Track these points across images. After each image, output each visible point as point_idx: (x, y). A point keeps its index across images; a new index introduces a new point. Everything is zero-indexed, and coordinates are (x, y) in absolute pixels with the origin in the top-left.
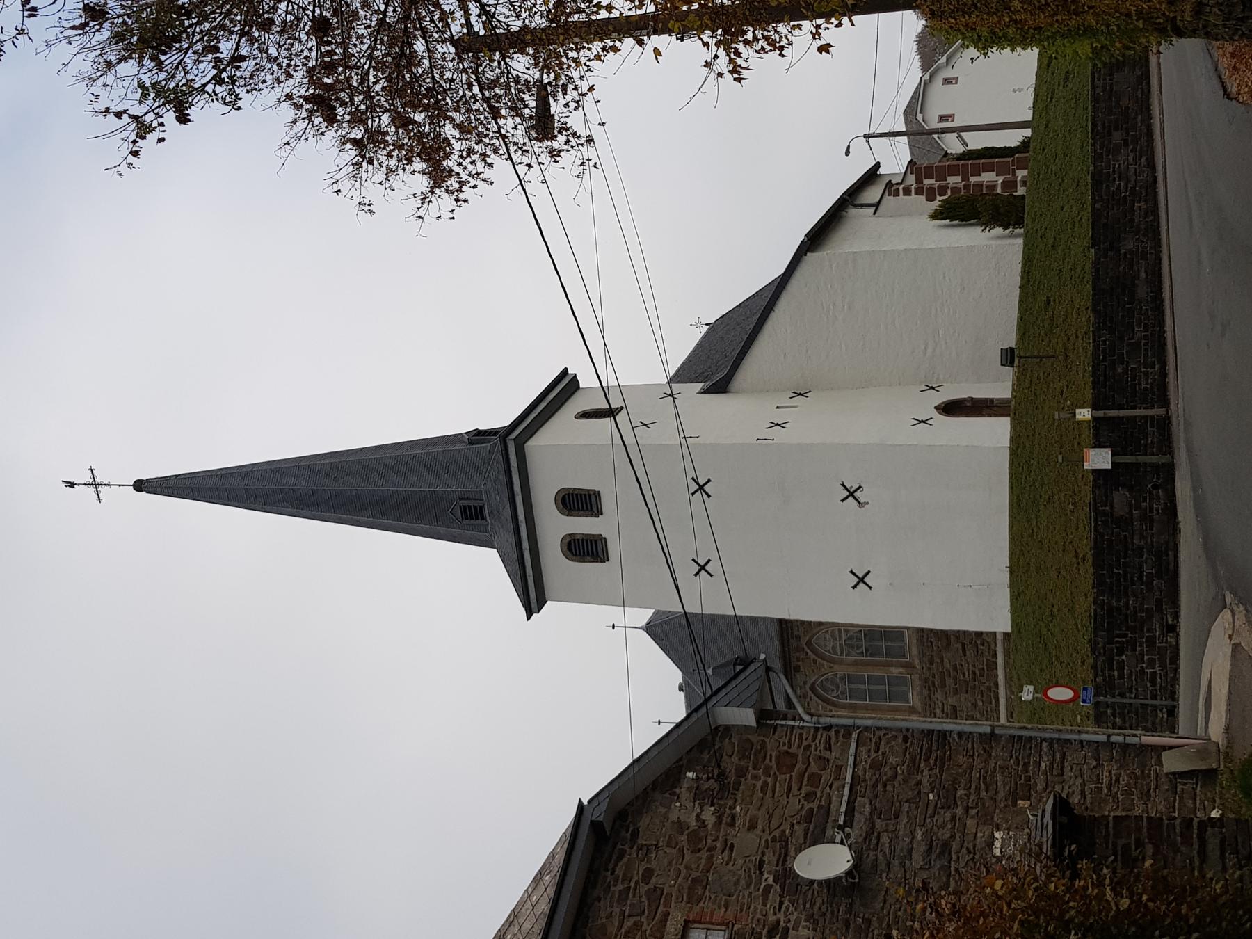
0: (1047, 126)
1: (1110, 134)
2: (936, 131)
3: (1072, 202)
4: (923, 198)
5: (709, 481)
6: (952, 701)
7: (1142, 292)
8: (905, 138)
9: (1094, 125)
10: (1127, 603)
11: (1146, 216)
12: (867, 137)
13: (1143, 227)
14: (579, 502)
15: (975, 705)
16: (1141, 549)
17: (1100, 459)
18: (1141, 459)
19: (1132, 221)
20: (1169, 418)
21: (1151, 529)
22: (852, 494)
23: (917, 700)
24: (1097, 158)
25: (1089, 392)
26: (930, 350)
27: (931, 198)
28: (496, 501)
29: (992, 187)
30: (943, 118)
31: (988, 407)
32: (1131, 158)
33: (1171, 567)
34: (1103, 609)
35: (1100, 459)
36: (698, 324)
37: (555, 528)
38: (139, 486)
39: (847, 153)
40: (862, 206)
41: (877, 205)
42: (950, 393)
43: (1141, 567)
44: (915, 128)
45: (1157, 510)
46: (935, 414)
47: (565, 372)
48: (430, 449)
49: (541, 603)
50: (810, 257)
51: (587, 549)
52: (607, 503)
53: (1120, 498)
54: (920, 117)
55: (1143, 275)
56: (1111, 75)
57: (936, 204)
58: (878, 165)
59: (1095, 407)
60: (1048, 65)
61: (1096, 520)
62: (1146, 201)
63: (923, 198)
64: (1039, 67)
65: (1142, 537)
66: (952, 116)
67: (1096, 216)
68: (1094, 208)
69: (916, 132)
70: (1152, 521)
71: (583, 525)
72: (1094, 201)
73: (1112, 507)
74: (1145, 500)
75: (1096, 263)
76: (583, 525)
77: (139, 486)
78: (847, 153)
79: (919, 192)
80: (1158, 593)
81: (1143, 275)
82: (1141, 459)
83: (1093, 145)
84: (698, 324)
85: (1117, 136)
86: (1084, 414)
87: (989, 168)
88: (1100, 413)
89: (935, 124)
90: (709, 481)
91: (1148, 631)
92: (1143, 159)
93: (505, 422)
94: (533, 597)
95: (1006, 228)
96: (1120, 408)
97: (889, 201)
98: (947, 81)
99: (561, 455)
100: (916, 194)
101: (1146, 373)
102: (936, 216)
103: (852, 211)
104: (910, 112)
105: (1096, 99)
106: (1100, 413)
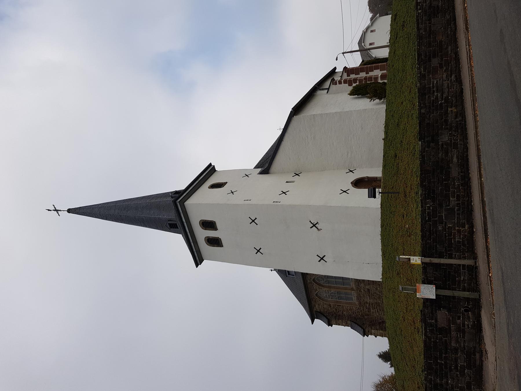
0: (394, 53)
1: (430, 60)
2: (369, 49)
3: (407, 101)
4: (347, 85)
5: (256, 218)
6: (367, 287)
7: (455, 172)
8: (359, 52)
9: (419, 55)
10: (447, 382)
11: (456, 117)
12: (343, 53)
13: (454, 125)
14: (209, 225)
15: (377, 289)
16: (456, 349)
17: (428, 292)
18: (458, 294)
19: (446, 121)
20: (476, 268)
21: (464, 337)
22: (314, 225)
23: (354, 285)
24: (422, 77)
25: (419, 248)
26: (349, 154)
27: (350, 85)
28: (179, 224)
29: (376, 78)
30: (371, 44)
31: (375, 181)
32: (445, 76)
33: (478, 363)
34: (431, 384)
35: (428, 292)
36: (280, 129)
37: (201, 234)
38: (69, 211)
39: (337, 59)
40: (323, 89)
41: (328, 89)
42: (359, 174)
43: (456, 360)
44: (362, 48)
45: (468, 325)
46: (350, 186)
47: (210, 165)
48: (159, 200)
49: (201, 261)
50: (295, 118)
51: (215, 242)
52: (218, 225)
53: (442, 315)
54: (363, 44)
55: (455, 160)
56: (430, 20)
57: (351, 88)
58: (335, 68)
59: (424, 254)
60: (395, 20)
61: (426, 329)
62: (456, 106)
63: (347, 85)
64: (392, 21)
65: (457, 342)
66: (374, 43)
67: (422, 118)
68: (420, 113)
69: (363, 50)
70: (464, 332)
71: (212, 234)
72: (420, 108)
73: (436, 321)
74: (459, 318)
75: (423, 151)
76: (212, 234)
77: (69, 211)
78: (337, 59)
79: (345, 82)
80: (468, 378)
81: (455, 160)
82: (458, 294)
83: (419, 69)
84: (280, 129)
85: (435, 62)
86: (416, 260)
87: (376, 68)
88: (427, 260)
89: (368, 47)
90: (256, 218)
91: (439, 213)
92: (453, 76)
93: (183, 188)
94: (198, 260)
95: (380, 99)
96: (441, 256)
97: (333, 87)
98: (372, 31)
99: (199, 206)
100: (344, 83)
101: (459, 231)
102: (351, 94)
103: (319, 92)
104: (360, 43)
105: (420, 37)
106: (427, 260)
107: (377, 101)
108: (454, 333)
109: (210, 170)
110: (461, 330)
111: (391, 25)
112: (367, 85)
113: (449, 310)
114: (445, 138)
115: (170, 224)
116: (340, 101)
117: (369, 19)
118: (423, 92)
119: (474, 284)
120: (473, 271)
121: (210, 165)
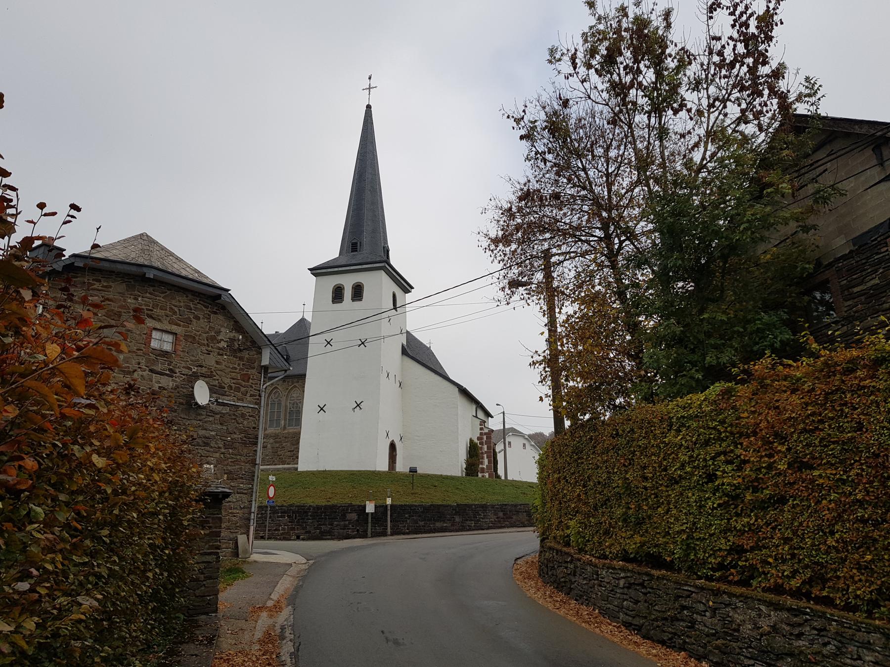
7: (438, 525)
14: (358, 292)
17: (370, 508)
18: (370, 525)
24: (493, 506)
25: (395, 503)
27: (478, 439)
28: (359, 257)
30: (510, 443)
35: (370, 508)
36: (430, 343)
37: (348, 282)
38: (369, 107)
41: (476, 417)
46: (391, 440)
49: (315, 275)
51: (338, 295)
52: (357, 304)
53: (354, 516)
57: (476, 441)
59: (391, 506)
65: (337, 525)
67: (469, 506)
69: (504, 432)
71: (348, 293)
75: (451, 506)
76: (348, 293)
77: (369, 107)
82: (370, 525)
84: (430, 343)
85: (501, 514)
87: (489, 462)
88: (389, 508)
93: (392, 263)
94: (318, 271)
97: (478, 422)
98: (524, 445)
99: (378, 286)
102: (471, 440)
103: (474, 407)
104: (513, 430)
106: (389, 508)
107: (465, 466)
108: (342, 523)
109: (406, 287)
110: (345, 527)
111: (526, 482)
112: (477, 455)
113: (357, 521)
114: (457, 519)
115: (356, 243)
116: (466, 430)
117: (538, 431)
118: (484, 507)
119: (375, 535)
120: (384, 534)
121: (412, 288)
